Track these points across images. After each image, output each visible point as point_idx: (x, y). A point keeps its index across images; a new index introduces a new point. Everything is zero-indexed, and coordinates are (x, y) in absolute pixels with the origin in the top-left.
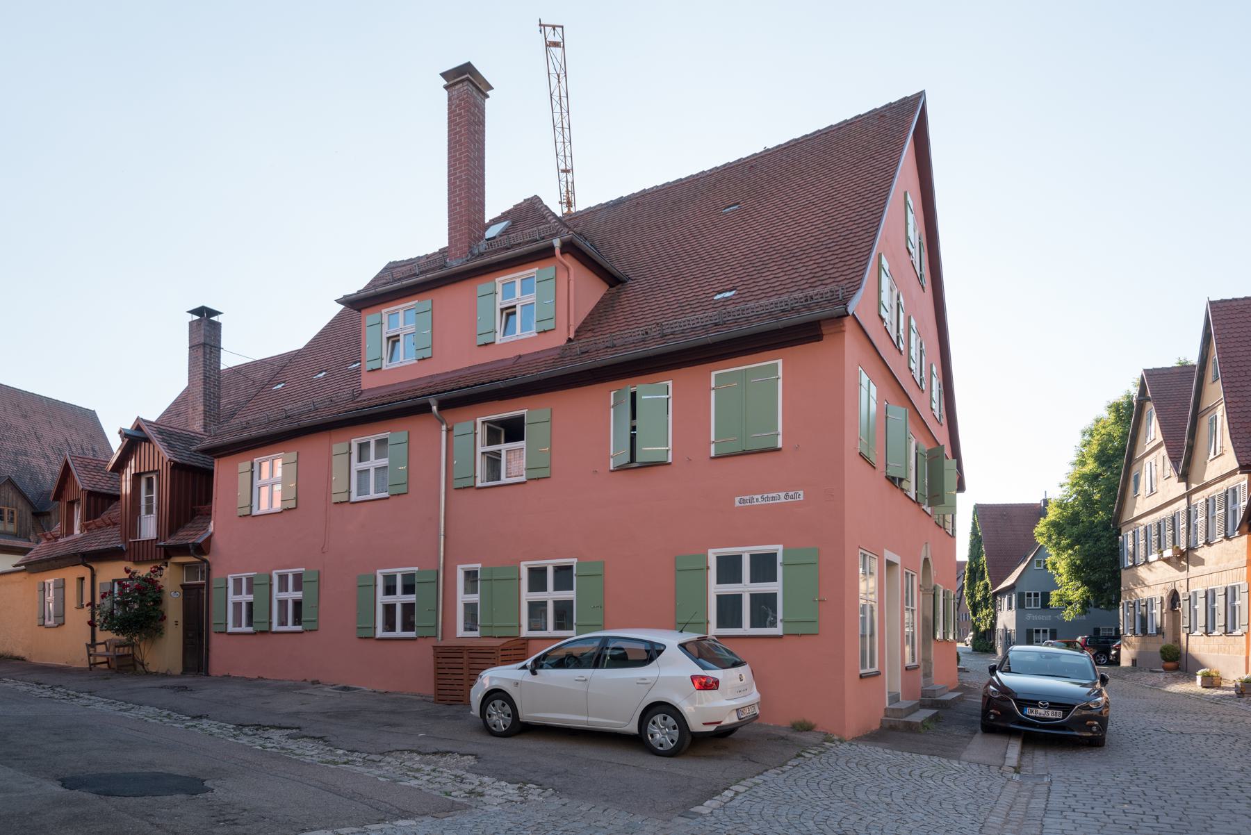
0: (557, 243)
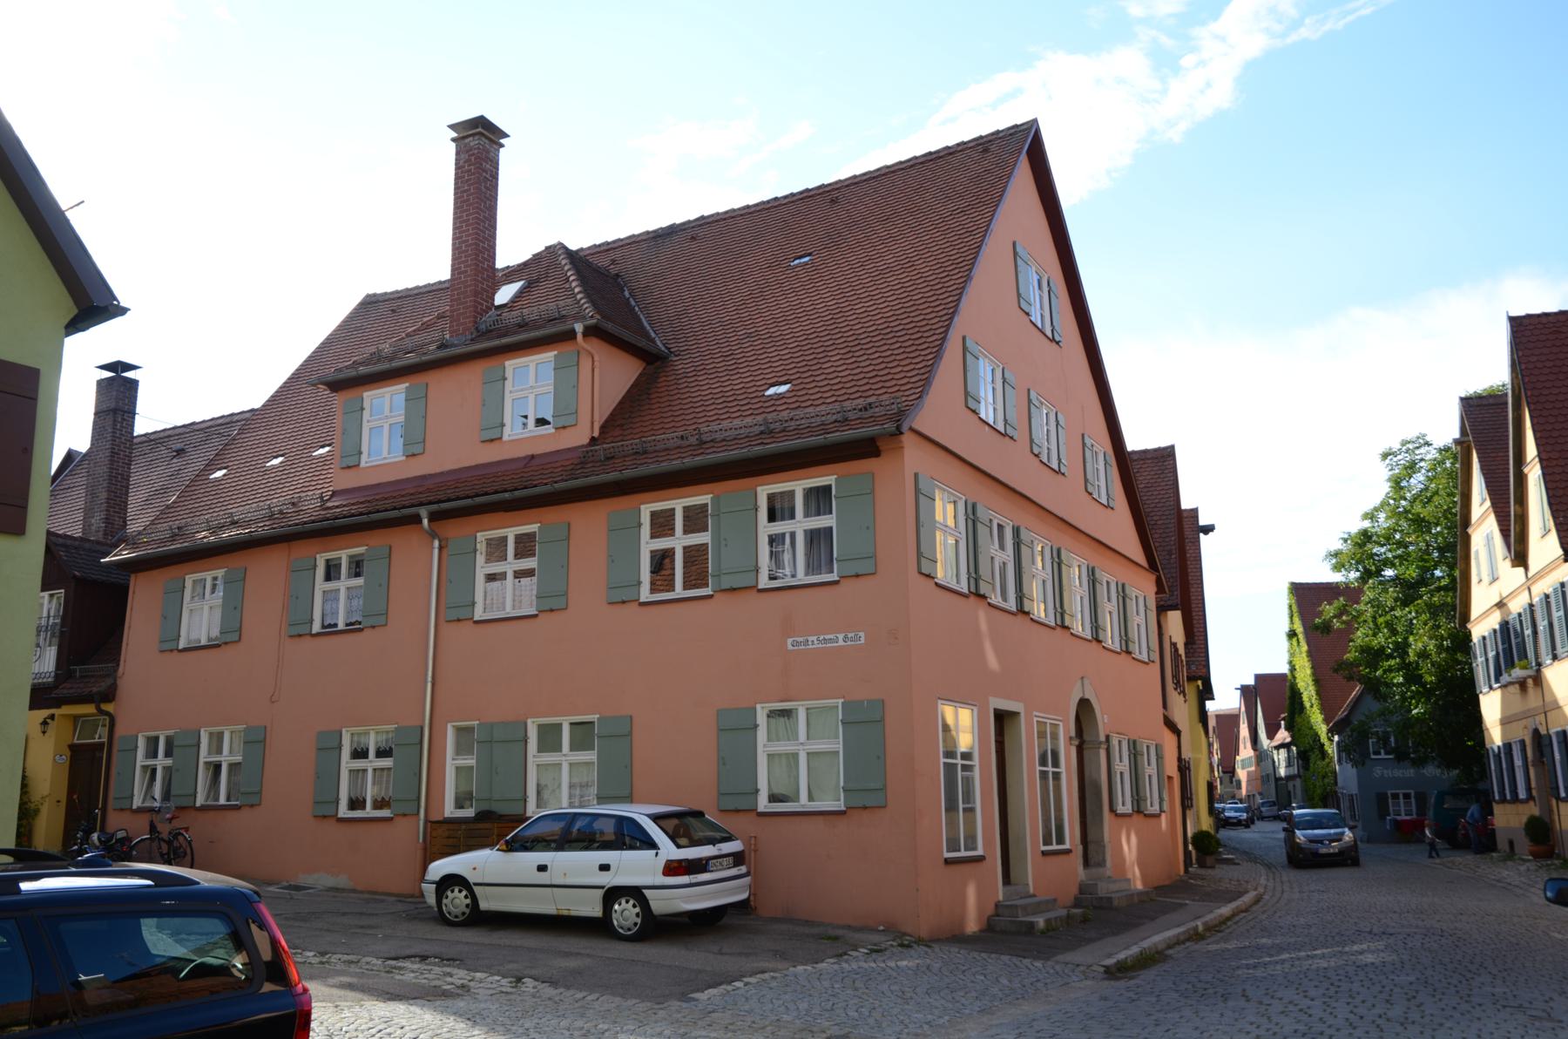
0: (579, 328)
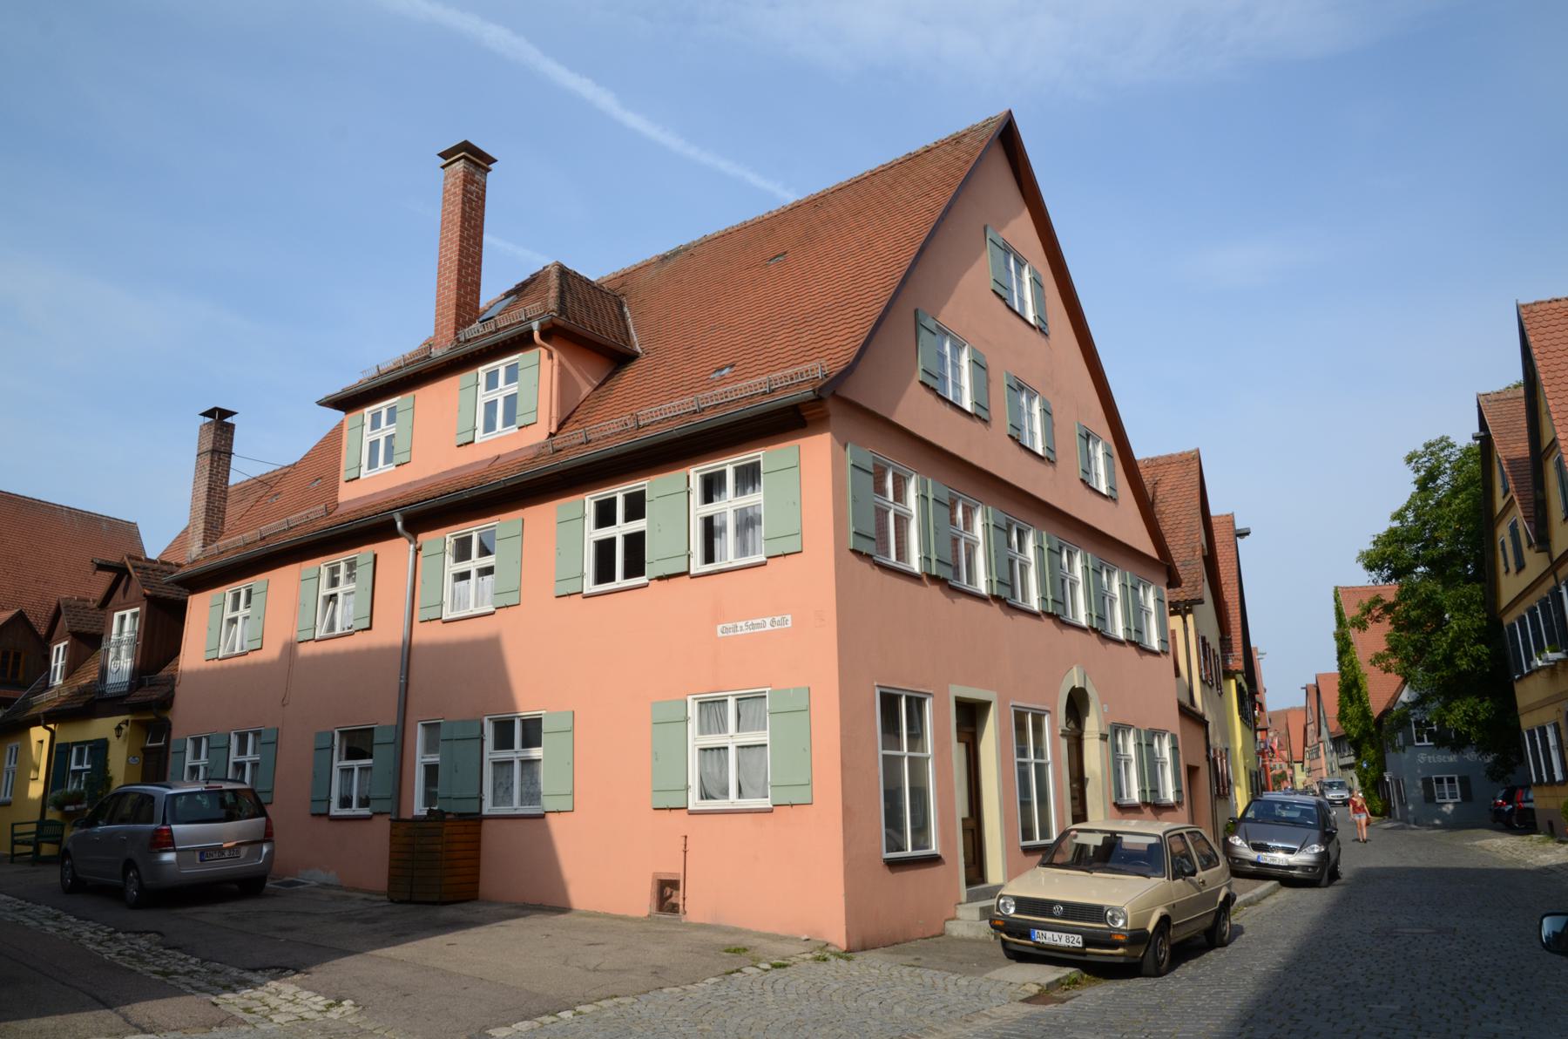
0: (535, 325)
